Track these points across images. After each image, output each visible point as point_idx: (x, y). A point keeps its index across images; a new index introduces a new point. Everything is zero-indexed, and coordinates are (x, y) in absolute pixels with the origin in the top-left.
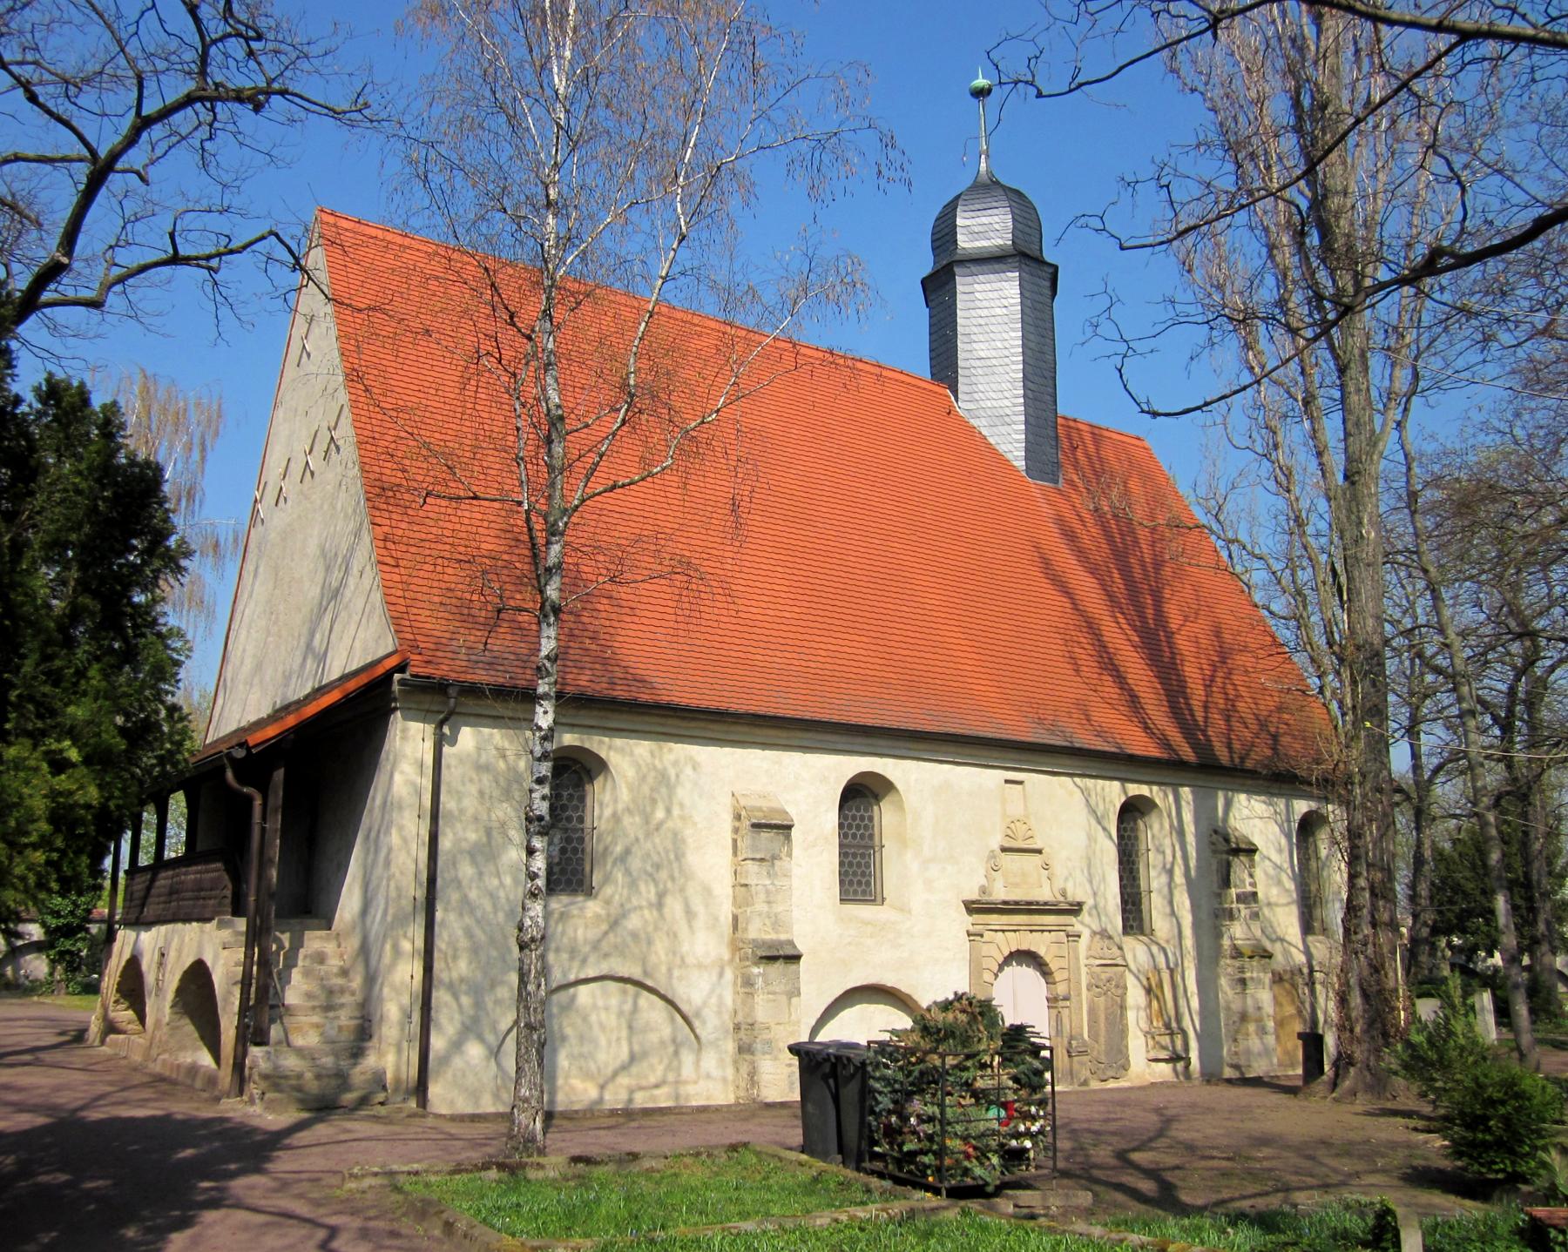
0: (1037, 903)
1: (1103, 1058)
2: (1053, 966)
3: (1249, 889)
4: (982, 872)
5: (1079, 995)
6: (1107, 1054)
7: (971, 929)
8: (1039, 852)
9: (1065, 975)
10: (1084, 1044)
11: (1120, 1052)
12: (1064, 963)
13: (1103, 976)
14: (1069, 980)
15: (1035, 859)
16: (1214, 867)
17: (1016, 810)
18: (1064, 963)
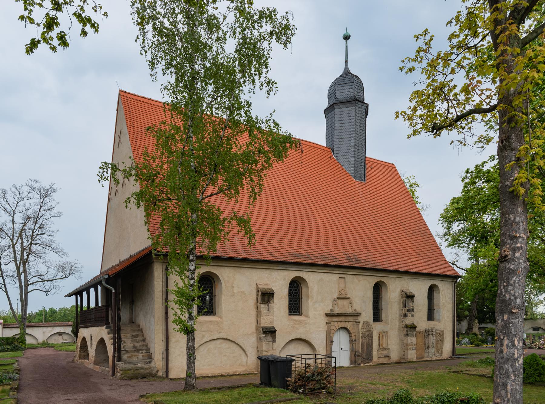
0: (347, 313)
1: (365, 357)
2: (351, 332)
3: (411, 308)
4: (331, 305)
5: (359, 339)
6: (366, 356)
7: (327, 321)
8: (349, 298)
9: (355, 334)
12: (354, 331)
13: (367, 334)
14: (356, 335)
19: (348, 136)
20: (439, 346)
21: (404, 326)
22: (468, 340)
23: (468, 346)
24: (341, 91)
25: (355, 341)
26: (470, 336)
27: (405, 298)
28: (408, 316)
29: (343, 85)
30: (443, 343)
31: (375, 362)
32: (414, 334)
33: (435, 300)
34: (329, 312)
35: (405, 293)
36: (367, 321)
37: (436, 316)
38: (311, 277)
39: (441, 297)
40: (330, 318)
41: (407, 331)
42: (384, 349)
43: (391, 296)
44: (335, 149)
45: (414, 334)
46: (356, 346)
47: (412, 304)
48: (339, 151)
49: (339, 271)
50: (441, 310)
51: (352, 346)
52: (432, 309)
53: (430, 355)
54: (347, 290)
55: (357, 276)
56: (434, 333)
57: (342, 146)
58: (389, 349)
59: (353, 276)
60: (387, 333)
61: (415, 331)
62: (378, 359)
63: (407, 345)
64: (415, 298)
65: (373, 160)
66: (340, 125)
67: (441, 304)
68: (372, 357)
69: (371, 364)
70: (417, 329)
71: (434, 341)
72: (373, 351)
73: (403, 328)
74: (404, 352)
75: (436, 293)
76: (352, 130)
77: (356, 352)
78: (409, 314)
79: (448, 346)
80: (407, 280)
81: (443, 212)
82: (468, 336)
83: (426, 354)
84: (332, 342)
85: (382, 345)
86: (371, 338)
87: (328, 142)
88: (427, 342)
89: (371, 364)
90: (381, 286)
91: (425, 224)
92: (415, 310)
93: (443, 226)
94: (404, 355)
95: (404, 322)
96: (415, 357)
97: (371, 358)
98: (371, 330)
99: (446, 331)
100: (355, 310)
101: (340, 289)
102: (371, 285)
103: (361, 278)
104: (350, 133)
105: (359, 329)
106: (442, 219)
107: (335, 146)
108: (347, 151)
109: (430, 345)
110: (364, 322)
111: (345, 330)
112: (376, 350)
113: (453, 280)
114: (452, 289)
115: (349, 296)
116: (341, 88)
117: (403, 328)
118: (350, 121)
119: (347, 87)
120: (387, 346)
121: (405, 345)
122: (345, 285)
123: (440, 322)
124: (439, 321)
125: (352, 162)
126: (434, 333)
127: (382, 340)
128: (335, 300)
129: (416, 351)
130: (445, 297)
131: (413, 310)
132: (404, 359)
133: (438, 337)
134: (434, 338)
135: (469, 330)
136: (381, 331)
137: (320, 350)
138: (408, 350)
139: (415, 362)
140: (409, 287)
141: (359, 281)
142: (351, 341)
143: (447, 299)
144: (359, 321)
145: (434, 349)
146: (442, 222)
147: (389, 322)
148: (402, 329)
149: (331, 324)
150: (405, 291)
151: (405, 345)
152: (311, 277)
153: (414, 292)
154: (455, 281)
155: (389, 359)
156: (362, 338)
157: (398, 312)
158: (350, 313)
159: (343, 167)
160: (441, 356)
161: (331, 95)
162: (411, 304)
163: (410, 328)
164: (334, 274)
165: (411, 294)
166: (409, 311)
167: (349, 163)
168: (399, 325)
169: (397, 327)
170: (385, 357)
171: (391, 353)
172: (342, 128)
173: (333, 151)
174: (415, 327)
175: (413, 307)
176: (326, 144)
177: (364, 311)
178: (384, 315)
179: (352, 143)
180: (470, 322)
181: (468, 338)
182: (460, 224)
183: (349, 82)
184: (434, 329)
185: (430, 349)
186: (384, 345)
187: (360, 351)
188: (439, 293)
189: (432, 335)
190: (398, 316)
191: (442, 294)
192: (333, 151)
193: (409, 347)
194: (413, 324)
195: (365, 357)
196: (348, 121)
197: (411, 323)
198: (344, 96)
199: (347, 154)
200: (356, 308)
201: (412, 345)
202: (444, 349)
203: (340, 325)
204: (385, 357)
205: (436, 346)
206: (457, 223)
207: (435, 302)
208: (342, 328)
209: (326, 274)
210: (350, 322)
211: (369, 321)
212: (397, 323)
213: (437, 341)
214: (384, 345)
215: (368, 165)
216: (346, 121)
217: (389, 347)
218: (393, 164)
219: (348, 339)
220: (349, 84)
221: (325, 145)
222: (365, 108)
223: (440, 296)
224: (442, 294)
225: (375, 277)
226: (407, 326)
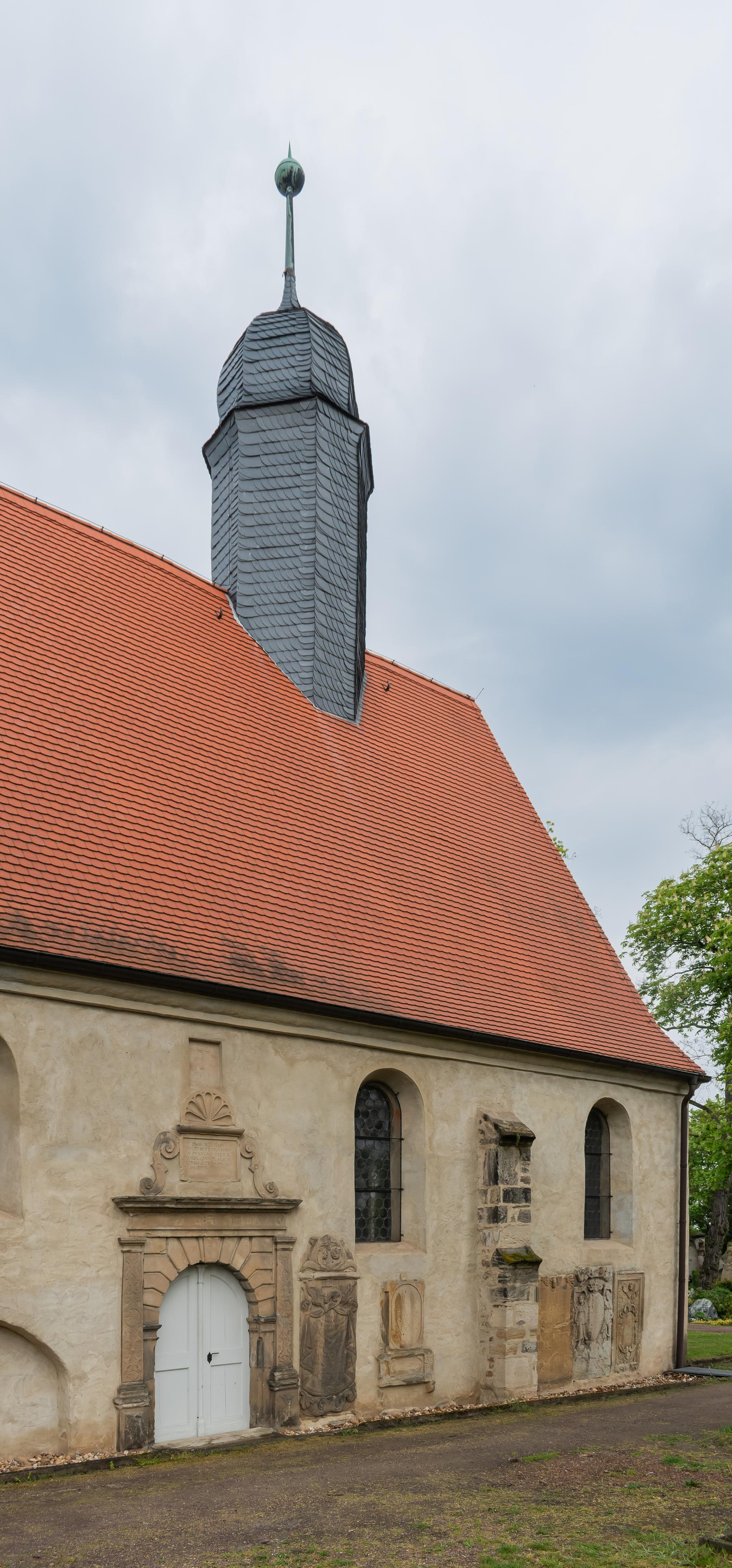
0: (228, 1201)
1: (319, 1390)
2: (253, 1283)
3: (520, 1185)
4: (147, 1160)
5: (290, 1315)
6: (325, 1384)
7: (126, 1236)
8: (239, 1134)
9: (269, 1292)
10: (294, 1376)
11: (344, 1380)
12: (267, 1278)
13: (327, 1292)
14: (274, 1298)
15: (233, 1147)
16: (481, 1160)
17: (205, 1078)
18: (267, 1278)
19: (288, 540)
20: (628, 1332)
21: (490, 1256)
22: (709, 1304)
23: (714, 1323)
24: (263, 364)
25: (272, 1320)
26: (714, 1292)
27: (493, 1146)
28: (504, 1219)
29: (270, 343)
30: (640, 1322)
31: (364, 1408)
32: (532, 1288)
33: (613, 1159)
34: (135, 1193)
35: (496, 1126)
36: (327, 1238)
37: (617, 1220)
38: (33, 1026)
39: (635, 1148)
40: (140, 1222)
41: (502, 1279)
42: (407, 1354)
43: (437, 1137)
44: (241, 589)
45: (532, 1290)
46: (274, 1342)
47: (525, 1170)
48: (257, 598)
49: (186, 1008)
50: (636, 1199)
51: (260, 1342)
52: (604, 1193)
53: (594, 1369)
54: (230, 1097)
55: (280, 1041)
56: (609, 1286)
57: (264, 576)
58: (429, 1351)
59: (262, 1038)
60: (418, 1286)
61: (534, 1276)
62: (380, 1395)
63: (503, 1334)
64: (534, 1147)
65: (391, 668)
66: (258, 494)
67: (636, 1177)
68: (352, 1388)
69: (346, 1418)
70: (543, 1270)
71: (609, 1314)
72: (359, 1361)
73: (485, 1264)
74: (491, 1360)
75: (618, 1134)
76: (305, 514)
77: (275, 1369)
78: (512, 1210)
79: (659, 1334)
80: (502, 1075)
81: (635, 921)
82: (710, 1293)
83: (578, 1367)
84: (152, 1329)
85: (397, 1336)
86: (346, 1310)
87: (219, 569)
88: (582, 1318)
89: (346, 1418)
90: (396, 1096)
91: (579, 896)
92: (534, 1195)
93: (636, 961)
94: (490, 1374)
95: (489, 1242)
96: (535, 1381)
97: (347, 1392)
98: (349, 1273)
99: (653, 1275)
100: (271, 1188)
101: (195, 1090)
102: (347, 1083)
103: (301, 1049)
104: (296, 527)
105: (288, 1272)
106: (632, 940)
107: (241, 577)
108: (286, 598)
109: (595, 1331)
110: (313, 1242)
111: (225, 1276)
112: (371, 1358)
113: (678, 1088)
114: (673, 1123)
115: (237, 1124)
116: (262, 355)
117: (485, 1264)
118: (297, 480)
119: (284, 351)
120: (421, 1338)
121: (493, 1334)
122: (222, 1076)
123: (630, 1244)
124: (628, 1239)
125: (304, 640)
126: (609, 1286)
127: (399, 1316)
128: (166, 1141)
129: (539, 1358)
130: (651, 1152)
131: (526, 1194)
132: (489, 1388)
133: (624, 1301)
134: (609, 1304)
135: (708, 1274)
136: (395, 1278)
137: (87, 1368)
138: (504, 1354)
139: (531, 1403)
140: (511, 1102)
141: (292, 1062)
142: (255, 1323)
143: (657, 1158)
144: (289, 1234)
145: (607, 1344)
146: (632, 950)
147: (430, 1243)
148: (482, 1270)
149: (146, 1250)
150: (494, 1115)
151: (493, 1334)
152: (33, 1026)
153: (532, 1123)
154: (686, 1092)
155: (430, 1392)
156: (304, 1306)
157: (466, 1203)
158: (242, 1201)
159: (272, 657)
160: (633, 1368)
161: (229, 389)
162: (518, 1168)
163: (515, 1265)
164: (163, 1024)
165: (517, 1130)
166: (509, 1196)
167: (293, 642)
168: (472, 1255)
169: (464, 1260)
170: (409, 1384)
171: (438, 1369)
172: (266, 506)
173: (233, 597)
174: (537, 1263)
175: (525, 1180)
176: (214, 569)
177: (312, 1193)
178: (407, 1213)
179: (306, 565)
180: (710, 1250)
181: (710, 1298)
182: (685, 957)
183: (293, 330)
184: (609, 1269)
185: (593, 1344)
186: (408, 1337)
187: (296, 1365)
188: (629, 1136)
189: (602, 1292)
190: (465, 1217)
191: (639, 1141)
192: (233, 597)
193: (509, 1344)
194: (527, 1249)
195: (319, 1390)
196: (289, 482)
197: (519, 1245)
198: (276, 387)
199: (286, 608)
200: (276, 1181)
201: (522, 1335)
202: (644, 1343)
203: (194, 1252)
204: (409, 1384)
205: (615, 1333)
206: (678, 956)
207: (614, 1171)
208: (192, 1268)
209: (115, 1018)
210: (245, 1241)
211: (337, 1236)
212: (464, 1248)
213: (622, 1314)
214: (408, 1337)
215: (371, 675)
216: (281, 482)
217: (429, 1343)
218: (468, 698)
219: (243, 1313)
220: (292, 339)
221: (208, 577)
222: (356, 439)
223: (630, 1147)
224: (639, 1141)
225: (367, 1053)
226: (500, 1258)
